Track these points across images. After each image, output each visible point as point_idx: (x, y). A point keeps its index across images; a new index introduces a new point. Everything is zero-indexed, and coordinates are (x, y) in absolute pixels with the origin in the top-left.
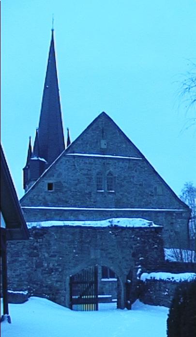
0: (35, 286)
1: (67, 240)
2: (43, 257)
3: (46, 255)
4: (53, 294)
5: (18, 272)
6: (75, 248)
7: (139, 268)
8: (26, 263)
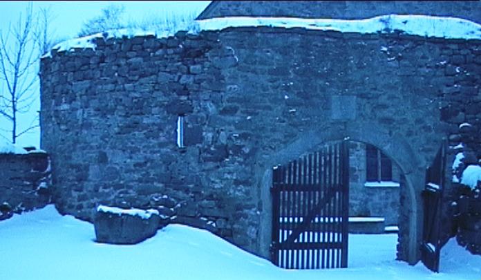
0: (181, 194)
1: (267, 68)
2: (203, 114)
3: (211, 108)
4: (227, 219)
6: (287, 89)
7: (460, 150)
8: (160, 130)
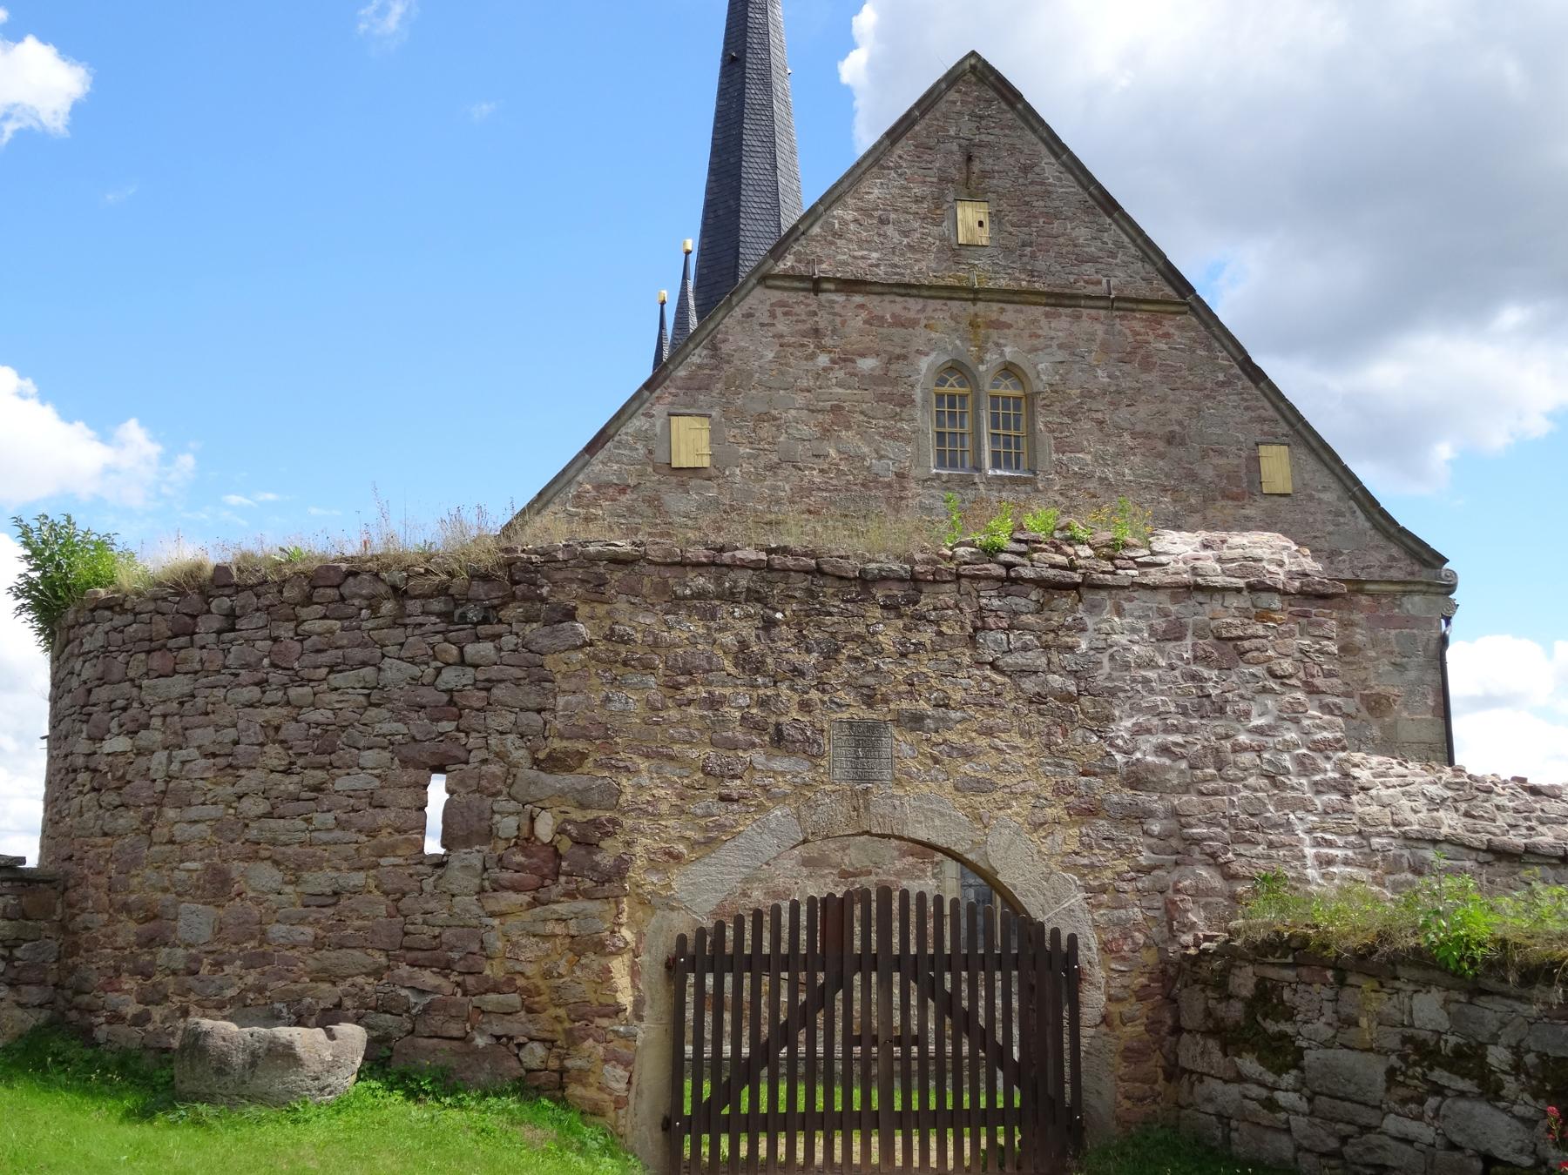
5: (319, 881)
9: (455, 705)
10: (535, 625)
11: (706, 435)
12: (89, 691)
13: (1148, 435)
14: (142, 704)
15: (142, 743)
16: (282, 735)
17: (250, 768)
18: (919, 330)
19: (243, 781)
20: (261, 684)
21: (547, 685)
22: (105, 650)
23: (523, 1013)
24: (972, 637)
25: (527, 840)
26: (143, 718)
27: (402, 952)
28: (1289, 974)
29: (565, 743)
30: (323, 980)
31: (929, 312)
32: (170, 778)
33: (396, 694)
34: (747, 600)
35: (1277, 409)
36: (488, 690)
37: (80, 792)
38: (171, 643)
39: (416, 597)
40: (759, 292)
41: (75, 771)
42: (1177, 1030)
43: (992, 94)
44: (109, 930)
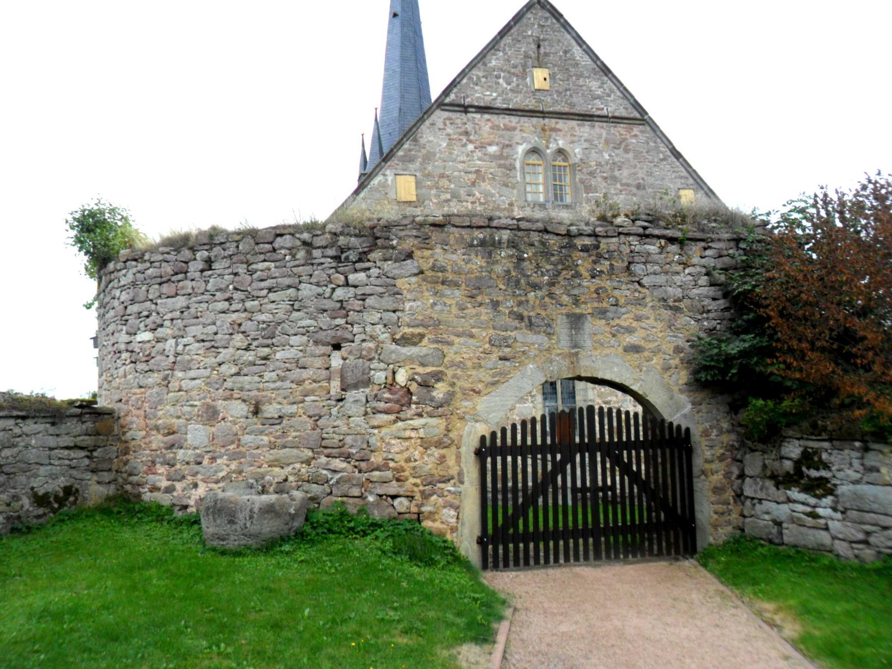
9: (344, 309)
10: (390, 262)
11: (413, 184)
12: (126, 308)
13: (628, 185)
14: (158, 313)
15: (160, 335)
16: (242, 329)
17: (225, 348)
18: (517, 132)
19: (221, 355)
20: (229, 300)
21: (399, 296)
22: (134, 284)
23: (394, 482)
24: (628, 268)
25: (391, 385)
26: (159, 321)
27: (322, 449)
28: (826, 445)
29: (411, 330)
30: (275, 466)
31: (522, 123)
32: (177, 354)
33: (309, 303)
34: (508, 247)
35: (688, 172)
36: (364, 300)
37: (124, 364)
38: (173, 278)
39: (319, 248)
40: (438, 113)
41: (119, 352)
42: (742, 476)
43: (548, 15)
44: (147, 440)
